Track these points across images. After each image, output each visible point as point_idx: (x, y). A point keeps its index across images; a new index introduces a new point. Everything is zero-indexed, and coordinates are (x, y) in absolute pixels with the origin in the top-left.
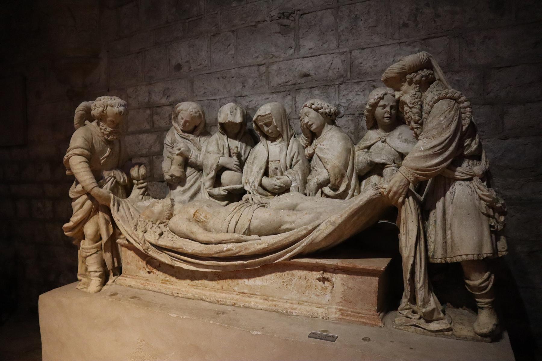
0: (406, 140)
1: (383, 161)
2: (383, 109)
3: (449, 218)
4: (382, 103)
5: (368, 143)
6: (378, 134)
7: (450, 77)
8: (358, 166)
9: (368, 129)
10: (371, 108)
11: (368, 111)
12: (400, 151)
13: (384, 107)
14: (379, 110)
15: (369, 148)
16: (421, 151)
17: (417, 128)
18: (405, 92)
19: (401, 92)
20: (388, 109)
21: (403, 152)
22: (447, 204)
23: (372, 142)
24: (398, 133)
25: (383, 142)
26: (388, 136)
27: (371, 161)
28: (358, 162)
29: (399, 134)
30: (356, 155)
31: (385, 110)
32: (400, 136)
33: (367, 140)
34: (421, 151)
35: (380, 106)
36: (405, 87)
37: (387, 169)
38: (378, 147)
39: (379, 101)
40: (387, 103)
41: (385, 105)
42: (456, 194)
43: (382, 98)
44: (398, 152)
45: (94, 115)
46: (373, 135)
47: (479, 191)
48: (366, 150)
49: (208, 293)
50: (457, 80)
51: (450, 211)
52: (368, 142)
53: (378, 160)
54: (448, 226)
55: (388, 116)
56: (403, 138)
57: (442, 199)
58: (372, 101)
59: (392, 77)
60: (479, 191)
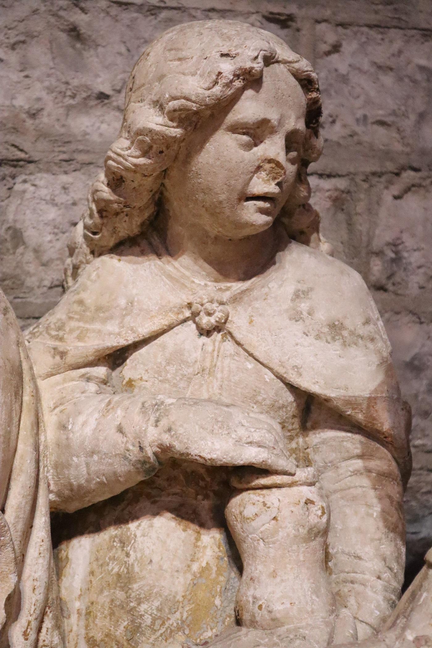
0: (335, 328)
1: (250, 455)
2: (248, 147)
4: (249, 108)
5: (114, 337)
6: (177, 282)
7: (400, 52)
8: (59, 467)
9: (97, 251)
10: (177, 132)
11: (150, 144)
12: (315, 389)
13: (256, 132)
14: (223, 150)
15: (116, 357)
20: (273, 147)
21: (331, 394)
23: (144, 331)
24: (290, 289)
25: (206, 332)
26: (236, 299)
27: (165, 449)
28: (64, 447)
29: (297, 295)
30: (47, 402)
31: (260, 151)
32: (304, 306)
33: (102, 312)
35: (235, 129)
37: (273, 497)
38: (177, 357)
39: (234, 99)
40: (273, 116)
41: (264, 123)
43: (251, 80)
44: (292, 388)
45: (139, 231)
46: (143, 289)
48: (101, 371)
49: (14, 428)
50: (422, 68)
52: (112, 327)
53: (215, 446)
55: (272, 188)
56: (321, 316)
58: (195, 87)
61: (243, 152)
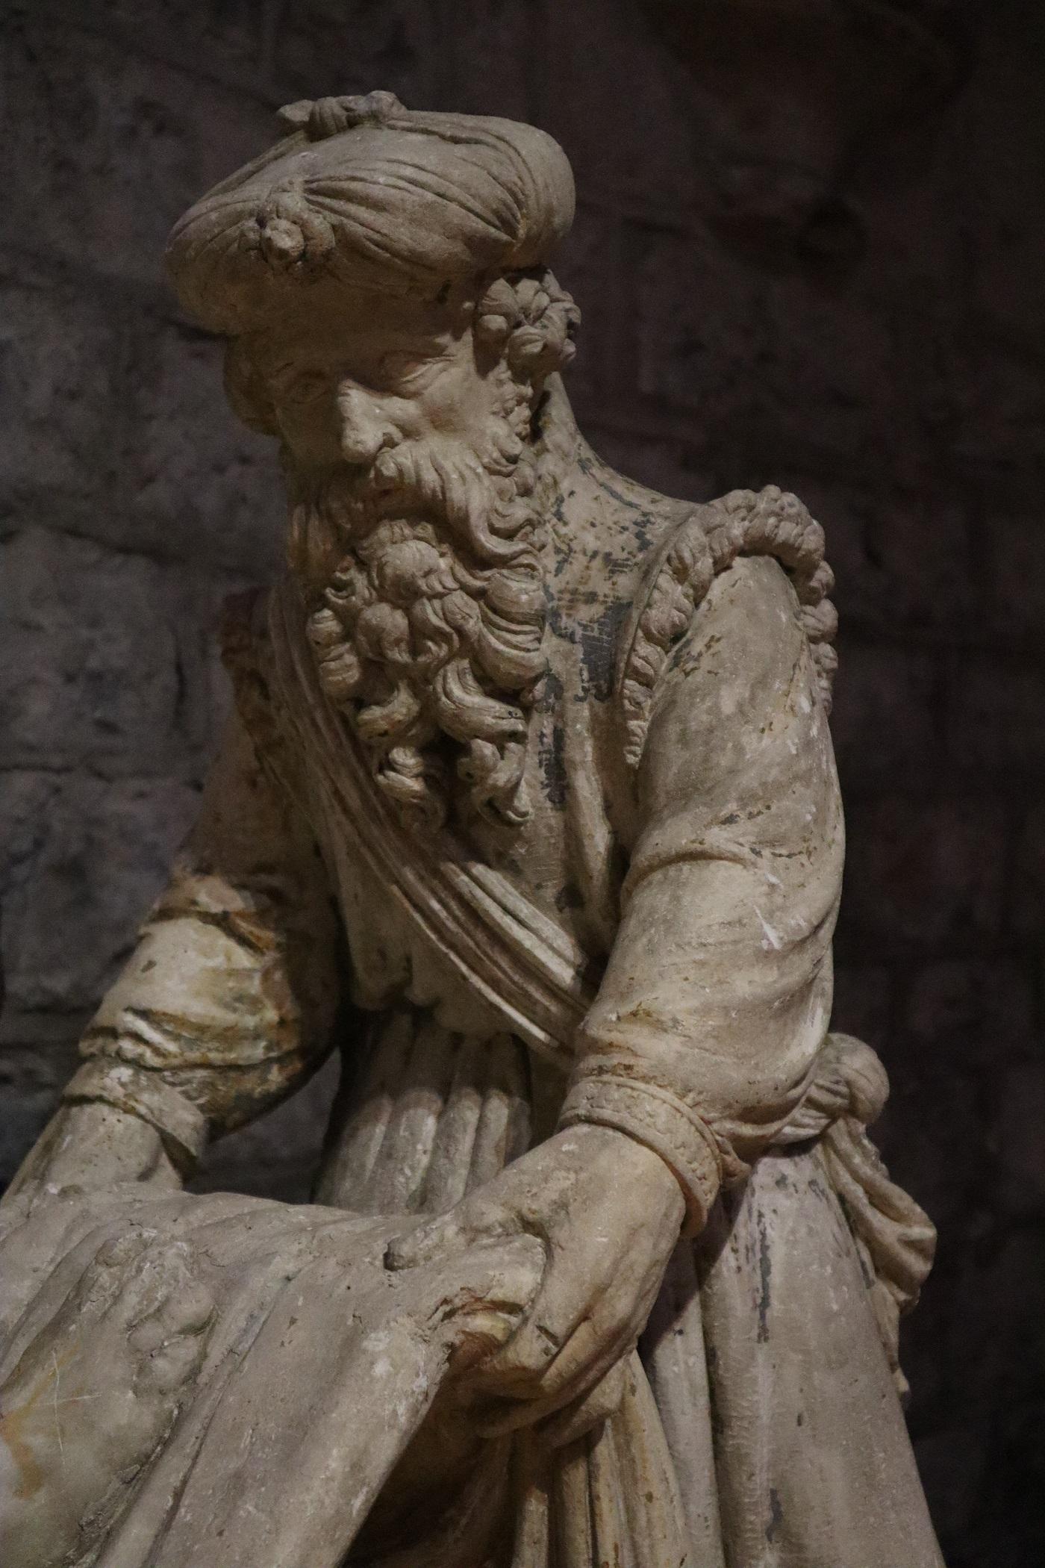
3: (758, 1449)
16: (766, 956)
17: (502, 739)
18: (443, 419)
19: (404, 408)
22: (735, 1343)
34: (766, 956)
36: (447, 374)
42: (777, 1255)
47: (876, 1219)
51: (763, 1392)
54: (758, 1517)
57: (693, 1310)
59: (416, 260)
60: (876, 1219)
61: (594, 507)
